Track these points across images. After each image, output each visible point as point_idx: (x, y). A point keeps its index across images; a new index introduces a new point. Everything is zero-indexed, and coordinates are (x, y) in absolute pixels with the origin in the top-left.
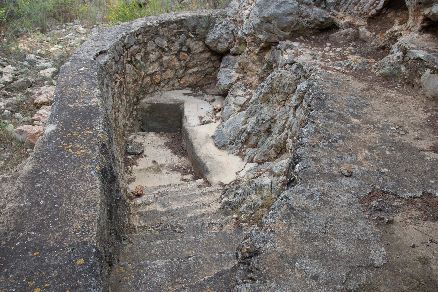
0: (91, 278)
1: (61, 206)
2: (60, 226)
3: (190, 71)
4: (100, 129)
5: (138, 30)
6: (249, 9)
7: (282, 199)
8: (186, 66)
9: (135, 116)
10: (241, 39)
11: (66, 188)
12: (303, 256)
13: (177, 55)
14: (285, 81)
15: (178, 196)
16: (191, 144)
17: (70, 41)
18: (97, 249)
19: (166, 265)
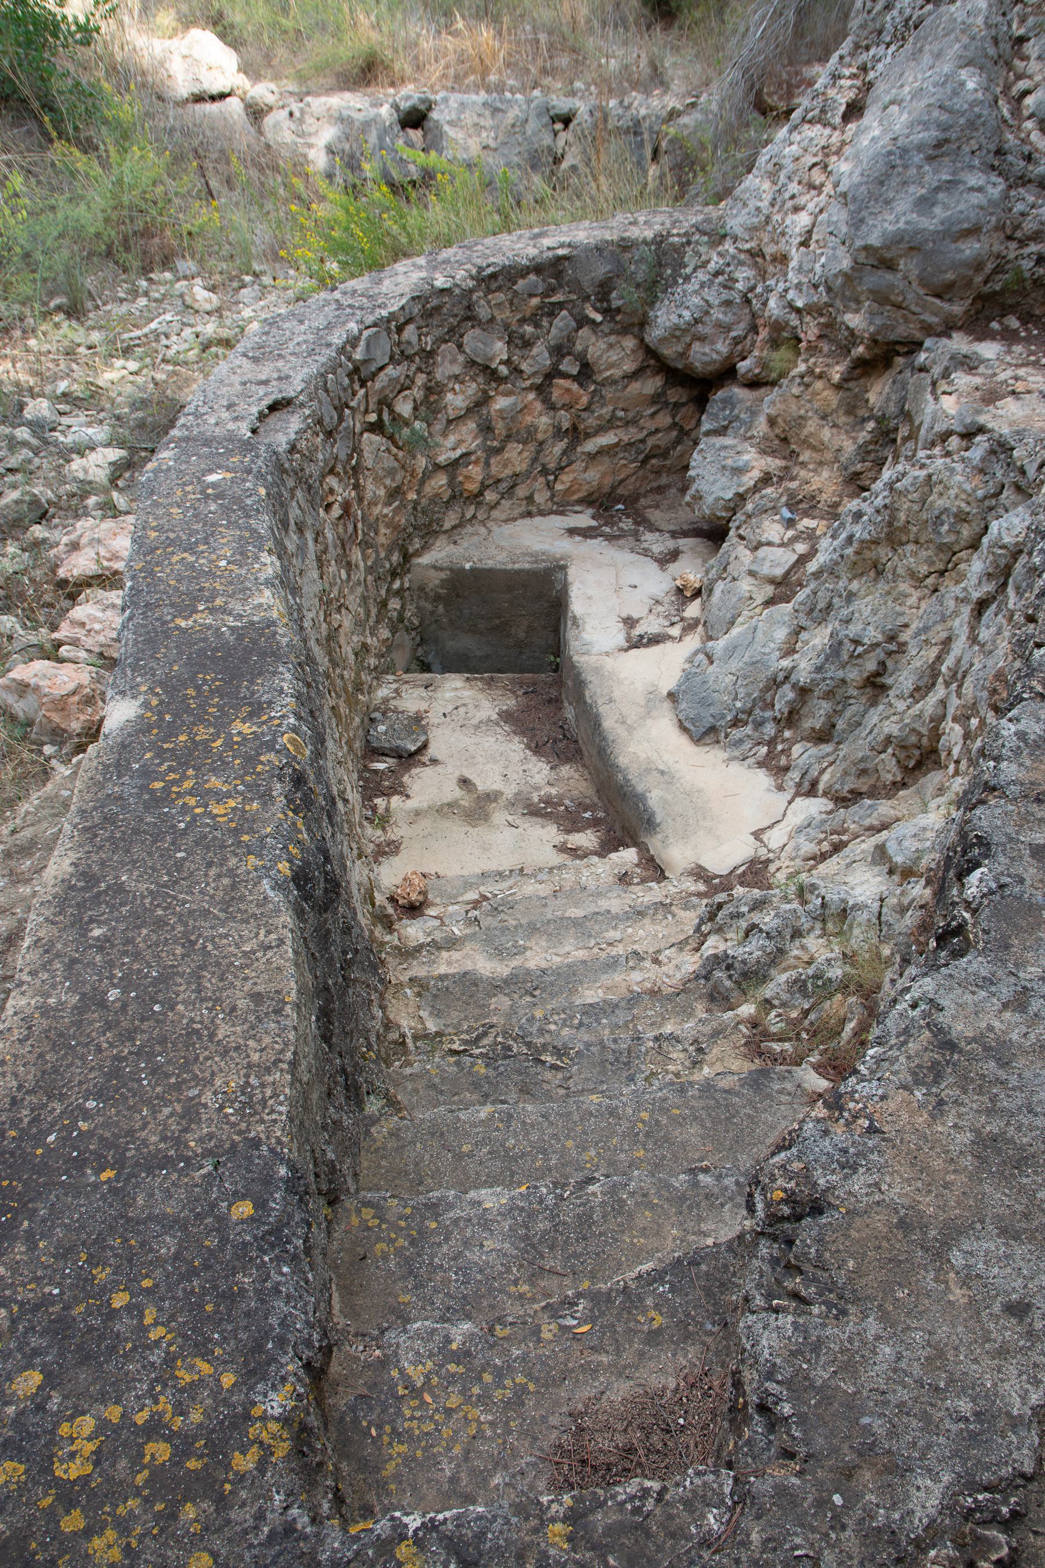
0: (278, 1265)
1: (172, 1008)
2: (173, 1080)
3: (590, 446)
4: (283, 716)
5: (403, 308)
6: (811, 206)
7: (914, 1006)
8: (575, 428)
9: (395, 614)
10: (777, 327)
11: (183, 946)
12: (979, 1226)
13: (542, 390)
14: (941, 503)
15: (549, 916)
16: (595, 723)
17: (164, 342)
18: (292, 1167)
19: (511, 1210)
